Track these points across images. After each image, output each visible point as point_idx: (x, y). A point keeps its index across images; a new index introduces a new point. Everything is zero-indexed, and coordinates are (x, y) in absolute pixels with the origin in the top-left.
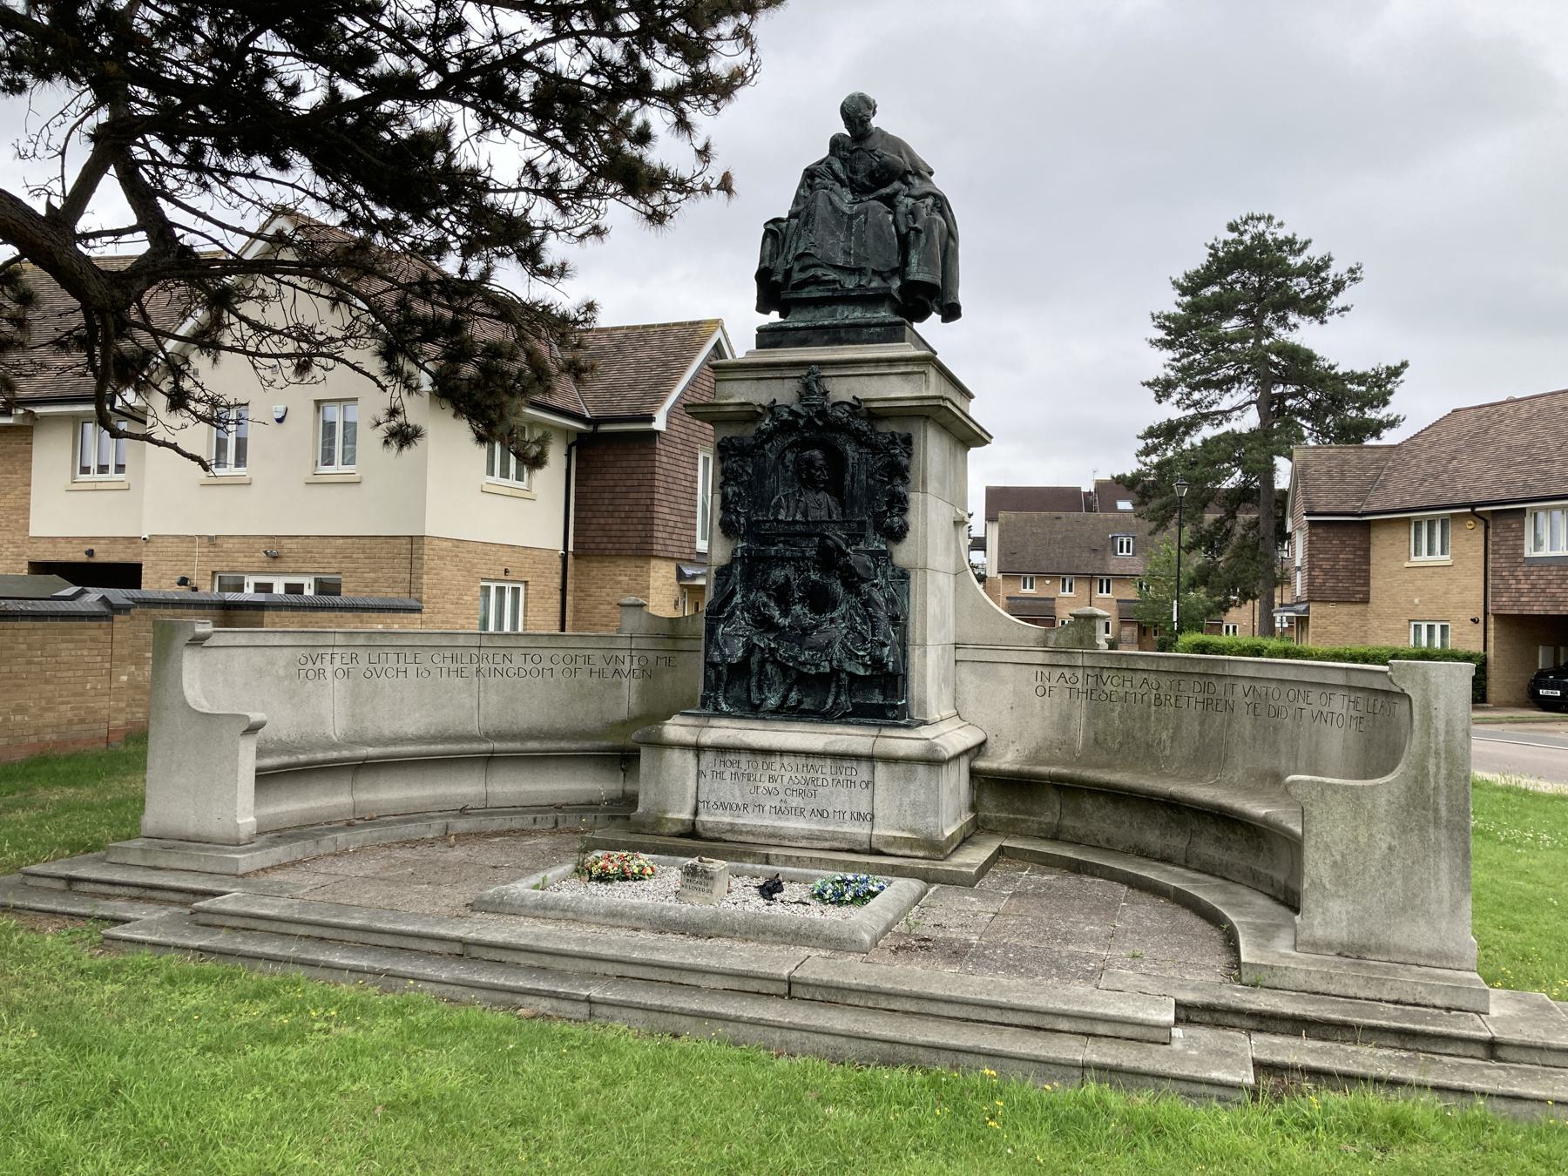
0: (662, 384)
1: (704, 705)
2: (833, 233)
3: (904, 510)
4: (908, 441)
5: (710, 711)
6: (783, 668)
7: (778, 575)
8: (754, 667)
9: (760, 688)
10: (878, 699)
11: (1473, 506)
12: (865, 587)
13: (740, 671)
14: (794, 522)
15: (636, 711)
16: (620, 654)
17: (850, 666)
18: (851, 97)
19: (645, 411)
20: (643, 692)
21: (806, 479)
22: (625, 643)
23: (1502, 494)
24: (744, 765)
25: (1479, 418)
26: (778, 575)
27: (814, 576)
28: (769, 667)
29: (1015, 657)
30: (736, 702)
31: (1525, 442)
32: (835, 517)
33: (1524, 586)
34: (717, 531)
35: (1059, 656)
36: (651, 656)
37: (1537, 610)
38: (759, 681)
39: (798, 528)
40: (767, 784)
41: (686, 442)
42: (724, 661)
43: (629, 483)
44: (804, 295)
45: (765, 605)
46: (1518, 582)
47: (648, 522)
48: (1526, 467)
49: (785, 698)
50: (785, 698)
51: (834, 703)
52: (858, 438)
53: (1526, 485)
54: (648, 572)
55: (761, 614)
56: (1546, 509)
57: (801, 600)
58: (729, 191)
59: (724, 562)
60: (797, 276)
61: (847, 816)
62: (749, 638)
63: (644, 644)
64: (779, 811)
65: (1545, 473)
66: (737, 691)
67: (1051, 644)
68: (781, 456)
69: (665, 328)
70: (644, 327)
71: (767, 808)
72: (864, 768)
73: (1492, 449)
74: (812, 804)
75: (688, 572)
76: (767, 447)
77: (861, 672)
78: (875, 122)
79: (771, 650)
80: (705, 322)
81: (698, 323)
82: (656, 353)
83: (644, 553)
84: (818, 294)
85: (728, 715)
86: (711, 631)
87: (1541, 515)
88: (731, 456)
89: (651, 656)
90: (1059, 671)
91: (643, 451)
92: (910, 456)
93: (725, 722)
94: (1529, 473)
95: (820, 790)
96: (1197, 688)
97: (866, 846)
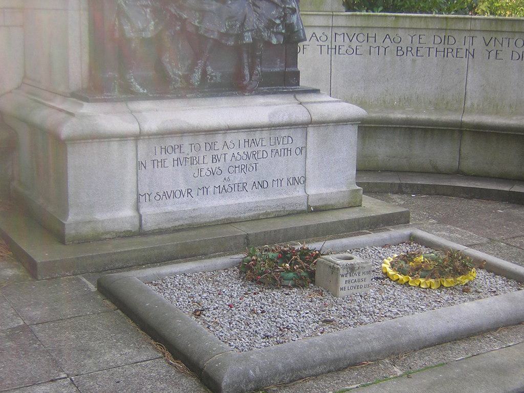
24: (186, 148)
40: (210, 165)
61: (284, 183)
64: (223, 190)
71: (211, 189)
72: (297, 135)
74: (250, 177)
85: (146, 98)
95: (261, 162)
96: (438, 40)
97: (304, 208)
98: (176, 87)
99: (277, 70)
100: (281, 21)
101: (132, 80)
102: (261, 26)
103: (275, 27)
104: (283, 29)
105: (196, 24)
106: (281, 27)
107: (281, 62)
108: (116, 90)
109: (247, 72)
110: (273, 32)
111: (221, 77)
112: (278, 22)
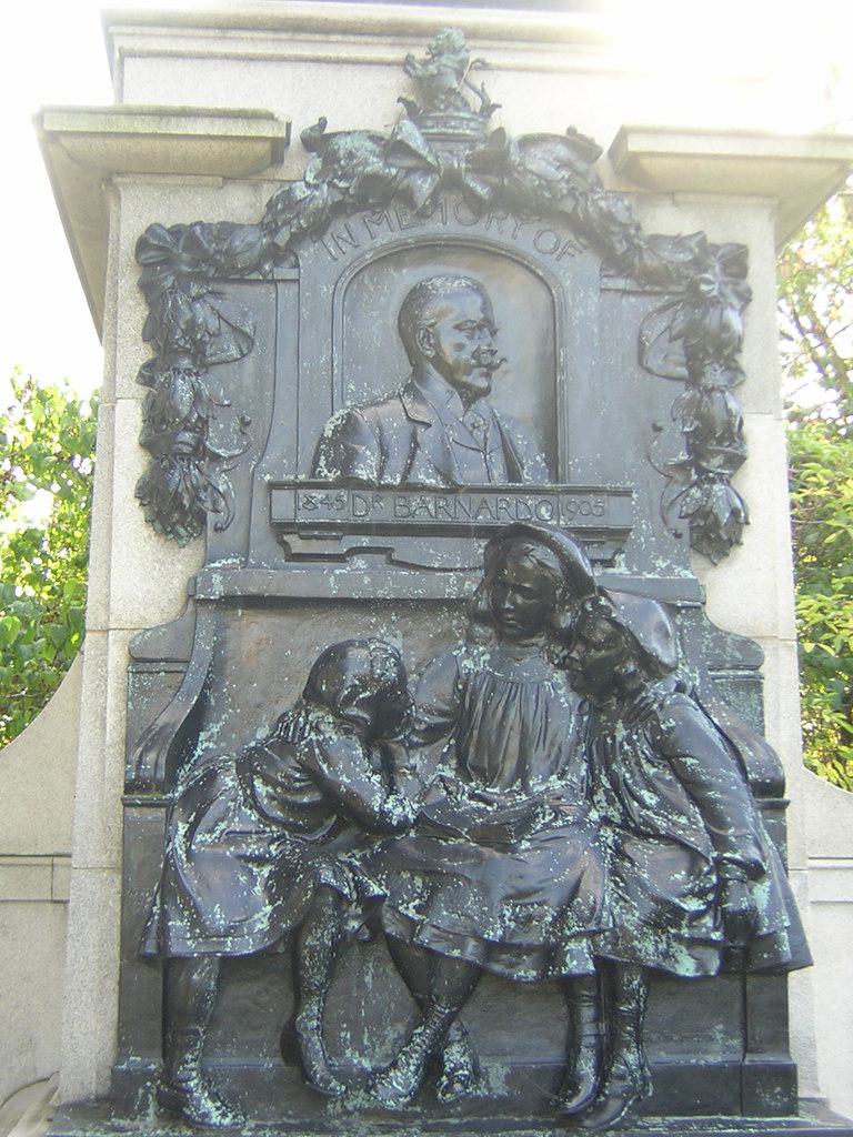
3: (736, 461)
12: (658, 690)
32: (527, 478)
39: (424, 510)
49: (432, 1066)
50: (432, 1066)
51: (603, 1073)
55: (315, 778)
79: (371, 904)
92: (745, 298)
98: (350, 1107)
99: (714, 1058)
100: (708, 904)
101: (192, 1084)
102: (632, 920)
103: (684, 923)
104: (716, 929)
105: (411, 913)
106: (708, 921)
107: (728, 1034)
108: (151, 1111)
109: (586, 1066)
110: (679, 938)
111: (509, 1080)
112: (693, 905)
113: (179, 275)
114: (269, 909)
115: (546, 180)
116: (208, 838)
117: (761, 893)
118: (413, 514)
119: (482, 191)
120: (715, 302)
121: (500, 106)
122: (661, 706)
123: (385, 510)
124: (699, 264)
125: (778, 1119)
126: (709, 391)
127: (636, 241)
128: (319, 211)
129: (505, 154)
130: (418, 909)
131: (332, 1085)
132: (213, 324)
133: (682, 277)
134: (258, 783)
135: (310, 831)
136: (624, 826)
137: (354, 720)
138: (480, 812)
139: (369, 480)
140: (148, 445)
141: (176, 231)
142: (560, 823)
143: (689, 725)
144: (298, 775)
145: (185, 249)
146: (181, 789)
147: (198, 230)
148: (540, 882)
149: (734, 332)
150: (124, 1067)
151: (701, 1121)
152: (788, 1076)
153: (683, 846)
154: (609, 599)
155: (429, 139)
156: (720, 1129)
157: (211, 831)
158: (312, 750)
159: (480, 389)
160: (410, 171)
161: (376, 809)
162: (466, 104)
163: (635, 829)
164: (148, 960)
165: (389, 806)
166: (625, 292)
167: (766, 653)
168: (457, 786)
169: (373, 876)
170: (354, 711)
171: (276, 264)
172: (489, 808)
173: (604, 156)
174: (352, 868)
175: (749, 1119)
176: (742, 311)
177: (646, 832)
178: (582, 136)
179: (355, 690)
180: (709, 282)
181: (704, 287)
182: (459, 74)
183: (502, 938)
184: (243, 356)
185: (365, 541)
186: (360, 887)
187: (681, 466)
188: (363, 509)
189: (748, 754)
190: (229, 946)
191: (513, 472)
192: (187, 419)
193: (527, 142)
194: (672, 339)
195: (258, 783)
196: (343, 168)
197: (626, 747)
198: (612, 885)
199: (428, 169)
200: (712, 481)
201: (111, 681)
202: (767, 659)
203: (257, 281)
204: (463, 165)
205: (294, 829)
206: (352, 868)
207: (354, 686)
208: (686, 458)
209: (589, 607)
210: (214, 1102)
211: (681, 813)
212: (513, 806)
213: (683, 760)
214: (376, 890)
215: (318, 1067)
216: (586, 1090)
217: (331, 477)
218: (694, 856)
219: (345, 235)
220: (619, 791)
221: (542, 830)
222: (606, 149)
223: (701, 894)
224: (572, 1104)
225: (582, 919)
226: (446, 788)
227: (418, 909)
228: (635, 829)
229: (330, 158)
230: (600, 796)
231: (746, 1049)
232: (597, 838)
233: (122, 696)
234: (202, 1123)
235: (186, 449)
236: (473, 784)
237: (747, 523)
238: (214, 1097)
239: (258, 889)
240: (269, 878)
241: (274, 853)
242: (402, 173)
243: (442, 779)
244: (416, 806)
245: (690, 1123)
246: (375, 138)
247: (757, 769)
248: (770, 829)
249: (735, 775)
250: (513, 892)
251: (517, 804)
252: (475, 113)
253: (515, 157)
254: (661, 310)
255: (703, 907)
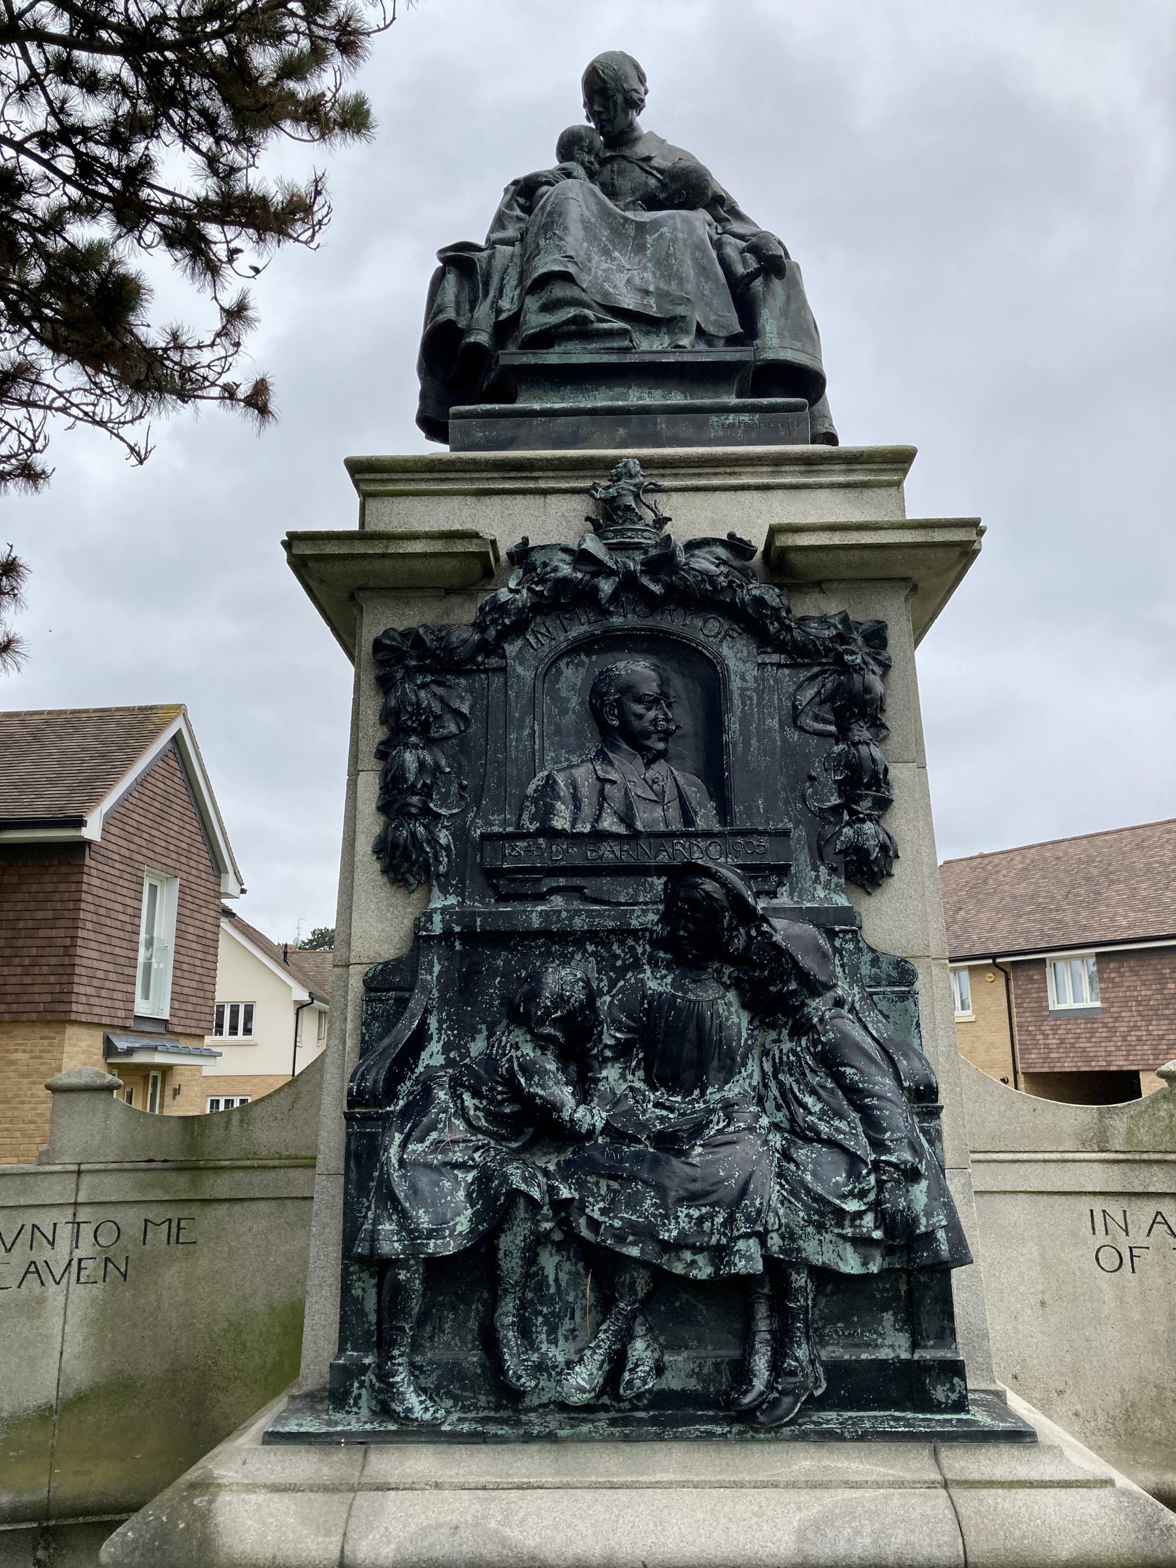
0: (98, 778)
1: (337, 1395)
2: (606, 252)
3: (884, 804)
4: (877, 637)
5: (355, 1422)
6: (601, 1264)
7: (563, 978)
8: (511, 1265)
9: (525, 1331)
10: (892, 1345)
11: (994, 956)
12: (818, 1007)
13: (468, 1275)
14: (598, 836)
15: (82, 1375)
16: (45, 1220)
17: (820, 1250)
18: (610, 55)
19: (71, 812)
20: (105, 1321)
21: (614, 725)
22: (60, 1190)
23: (1021, 945)
25: (974, 869)
26: (563, 978)
27: (656, 983)
28: (549, 1261)
29: (1036, 1178)
30: (444, 1384)
31: (1029, 891)
32: (701, 824)
33: (1053, 1042)
34: (369, 868)
35: (1144, 1173)
36: (130, 1219)
37: (1068, 1066)
38: (523, 1305)
39: (609, 852)
41: (127, 860)
42: (414, 1250)
43: (40, 915)
44: (552, 357)
45: (528, 1069)
46: (1046, 1037)
47: (67, 970)
48: (1038, 916)
49: (617, 1362)
50: (617, 1362)
51: (776, 1368)
52: (754, 624)
53: (1043, 935)
54: (61, 1045)
55: (515, 1092)
56: (1066, 959)
57: (622, 1051)
58: (263, 410)
59: (388, 952)
60: (536, 321)
62: (485, 1177)
63: (112, 1187)
65: (1060, 922)
66: (456, 1347)
67: (1117, 1143)
68: (549, 670)
69: (104, 715)
70: (74, 712)
73: (996, 898)
75: (121, 1044)
76: (511, 649)
77: (851, 1264)
78: (644, 121)
79: (560, 1206)
80: (162, 707)
81: (151, 708)
82: (91, 742)
83: (56, 1016)
84: (587, 359)
85: (430, 1434)
86: (362, 1156)
87: (1060, 965)
88: (410, 673)
89: (130, 1219)
90: (1149, 1208)
91: (64, 869)
92: (886, 667)
93: (419, 1462)
94: (1042, 922)
99: (885, 1354)
101: (398, 1379)
104: (876, 1228)
105: (596, 1215)
106: (869, 1220)
112: (852, 1206)
113: (407, 668)
114: (469, 1212)
115: (708, 576)
116: (419, 1147)
117: (920, 1192)
118: (601, 857)
119: (656, 588)
120: (858, 670)
121: (670, 519)
122: (821, 1020)
123: (575, 855)
124: (841, 638)
125: (948, 1417)
126: (855, 745)
127: (787, 622)
128: (520, 611)
129: (673, 554)
130: (603, 1212)
131: (523, 1380)
132: (437, 708)
133: (828, 651)
134: (466, 1096)
135: (509, 1140)
136: (792, 1131)
137: (549, 1038)
138: (662, 1119)
139: (564, 829)
140: (384, 808)
141: (404, 635)
142: (732, 1129)
143: (845, 1036)
144: (500, 1089)
145: (412, 647)
146: (401, 1103)
147: (421, 631)
148: (713, 1184)
149: (876, 694)
150: (341, 1362)
151: (875, 1417)
152: (956, 1369)
153: (844, 1150)
154: (771, 926)
155: (611, 548)
156: (891, 1427)
157: (421, 1140)
158: (511, 1067)
159: (658, 751)
160: (595, 575)
161: (567, 1118)
162: (641, 518)
163: (800, 1133)
164: (362, 1260)
165: (577, 1116)
166: (779, 666)
167: (919, 971)
168: (644, 1095)
169: (564, 1180)
170: (548, 1030)
171: (487, 657)
172: (671, 1116)
173: (758, 555)
174: (546, 1173)
175: (921, 1416)
176: (884, 676)
177: (808, 1135)
178: (741, 540)
179: (548, 1011)
180: (853, 653)
181: (847, 658)
182: (637, 497)
183: (676, 1239)
184: (461, 732)
185: (562, 882)
186: (552, 1190)
187: (836, 810)
188: (560, 854)
189: (903, 1064)
190: (432, 1246)
191: (687, 817)
192: (413, 785)
193: (693, 546)
194: (821, 703)
195: (466, 1096)
196: (538, 575)
197: (792, 1058)
198: (777, 1187)
199: (609, 573)
200: (863, 821)
201: (350, 1008)
202: (920, 977)
203: (472, 671)
204: (639, 568)
205: (499, 1138)
206: (546, 1173)
207: (547, 1007)
208: (838, 801)
209: (753, 933)
210: (419, 1395)
211: (842, 1117)
212: (691, 1113)
213: (843, 1069)
214: (565, 1193)
215: (510, 1362)
216: (759, 1384)
217: (533, 828)
218: (854, 1161)
219: (543, 631)
220: (787, 1098)
221: (715, 1135)
222: (761, 548)
223: (862, 1194)
224: (747, 1399)
225: (749, 1219)
226: (634, 1098)
227: (603, 1212)
228: (800, 1133)
229: (529, 568)
230: (770, 1105)
231: (914, 1346)
232: (766, 1142)
233: (358, 1022)
234: (407, 1418)
235: (414, 810)
236: (658, 1093)
237: (897, 857)
238: (421, 1390)
239: (461, 1194)
240: (472, 1183)
241: (477, 1159)
242: (587, 577)
243: (631, 1089)
244: (604, 1115)
245: (862, 1419)
246: (566, 550)
247: (911, 1076)
248: (925, 1132)
249: (889, 1082)
250: (685, 1194)
251: (695, 1112)
252: (647, 525)
253: (682, 558)
254: (812, 678)
255: (863, 1208)
